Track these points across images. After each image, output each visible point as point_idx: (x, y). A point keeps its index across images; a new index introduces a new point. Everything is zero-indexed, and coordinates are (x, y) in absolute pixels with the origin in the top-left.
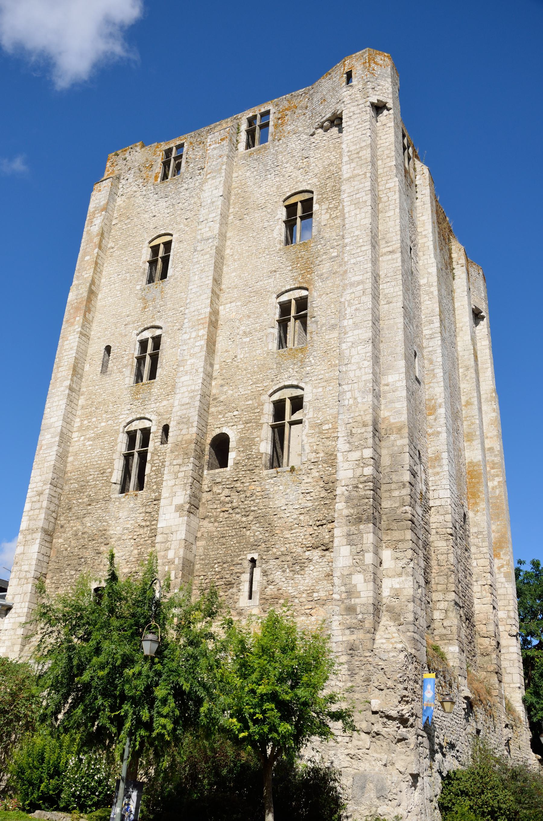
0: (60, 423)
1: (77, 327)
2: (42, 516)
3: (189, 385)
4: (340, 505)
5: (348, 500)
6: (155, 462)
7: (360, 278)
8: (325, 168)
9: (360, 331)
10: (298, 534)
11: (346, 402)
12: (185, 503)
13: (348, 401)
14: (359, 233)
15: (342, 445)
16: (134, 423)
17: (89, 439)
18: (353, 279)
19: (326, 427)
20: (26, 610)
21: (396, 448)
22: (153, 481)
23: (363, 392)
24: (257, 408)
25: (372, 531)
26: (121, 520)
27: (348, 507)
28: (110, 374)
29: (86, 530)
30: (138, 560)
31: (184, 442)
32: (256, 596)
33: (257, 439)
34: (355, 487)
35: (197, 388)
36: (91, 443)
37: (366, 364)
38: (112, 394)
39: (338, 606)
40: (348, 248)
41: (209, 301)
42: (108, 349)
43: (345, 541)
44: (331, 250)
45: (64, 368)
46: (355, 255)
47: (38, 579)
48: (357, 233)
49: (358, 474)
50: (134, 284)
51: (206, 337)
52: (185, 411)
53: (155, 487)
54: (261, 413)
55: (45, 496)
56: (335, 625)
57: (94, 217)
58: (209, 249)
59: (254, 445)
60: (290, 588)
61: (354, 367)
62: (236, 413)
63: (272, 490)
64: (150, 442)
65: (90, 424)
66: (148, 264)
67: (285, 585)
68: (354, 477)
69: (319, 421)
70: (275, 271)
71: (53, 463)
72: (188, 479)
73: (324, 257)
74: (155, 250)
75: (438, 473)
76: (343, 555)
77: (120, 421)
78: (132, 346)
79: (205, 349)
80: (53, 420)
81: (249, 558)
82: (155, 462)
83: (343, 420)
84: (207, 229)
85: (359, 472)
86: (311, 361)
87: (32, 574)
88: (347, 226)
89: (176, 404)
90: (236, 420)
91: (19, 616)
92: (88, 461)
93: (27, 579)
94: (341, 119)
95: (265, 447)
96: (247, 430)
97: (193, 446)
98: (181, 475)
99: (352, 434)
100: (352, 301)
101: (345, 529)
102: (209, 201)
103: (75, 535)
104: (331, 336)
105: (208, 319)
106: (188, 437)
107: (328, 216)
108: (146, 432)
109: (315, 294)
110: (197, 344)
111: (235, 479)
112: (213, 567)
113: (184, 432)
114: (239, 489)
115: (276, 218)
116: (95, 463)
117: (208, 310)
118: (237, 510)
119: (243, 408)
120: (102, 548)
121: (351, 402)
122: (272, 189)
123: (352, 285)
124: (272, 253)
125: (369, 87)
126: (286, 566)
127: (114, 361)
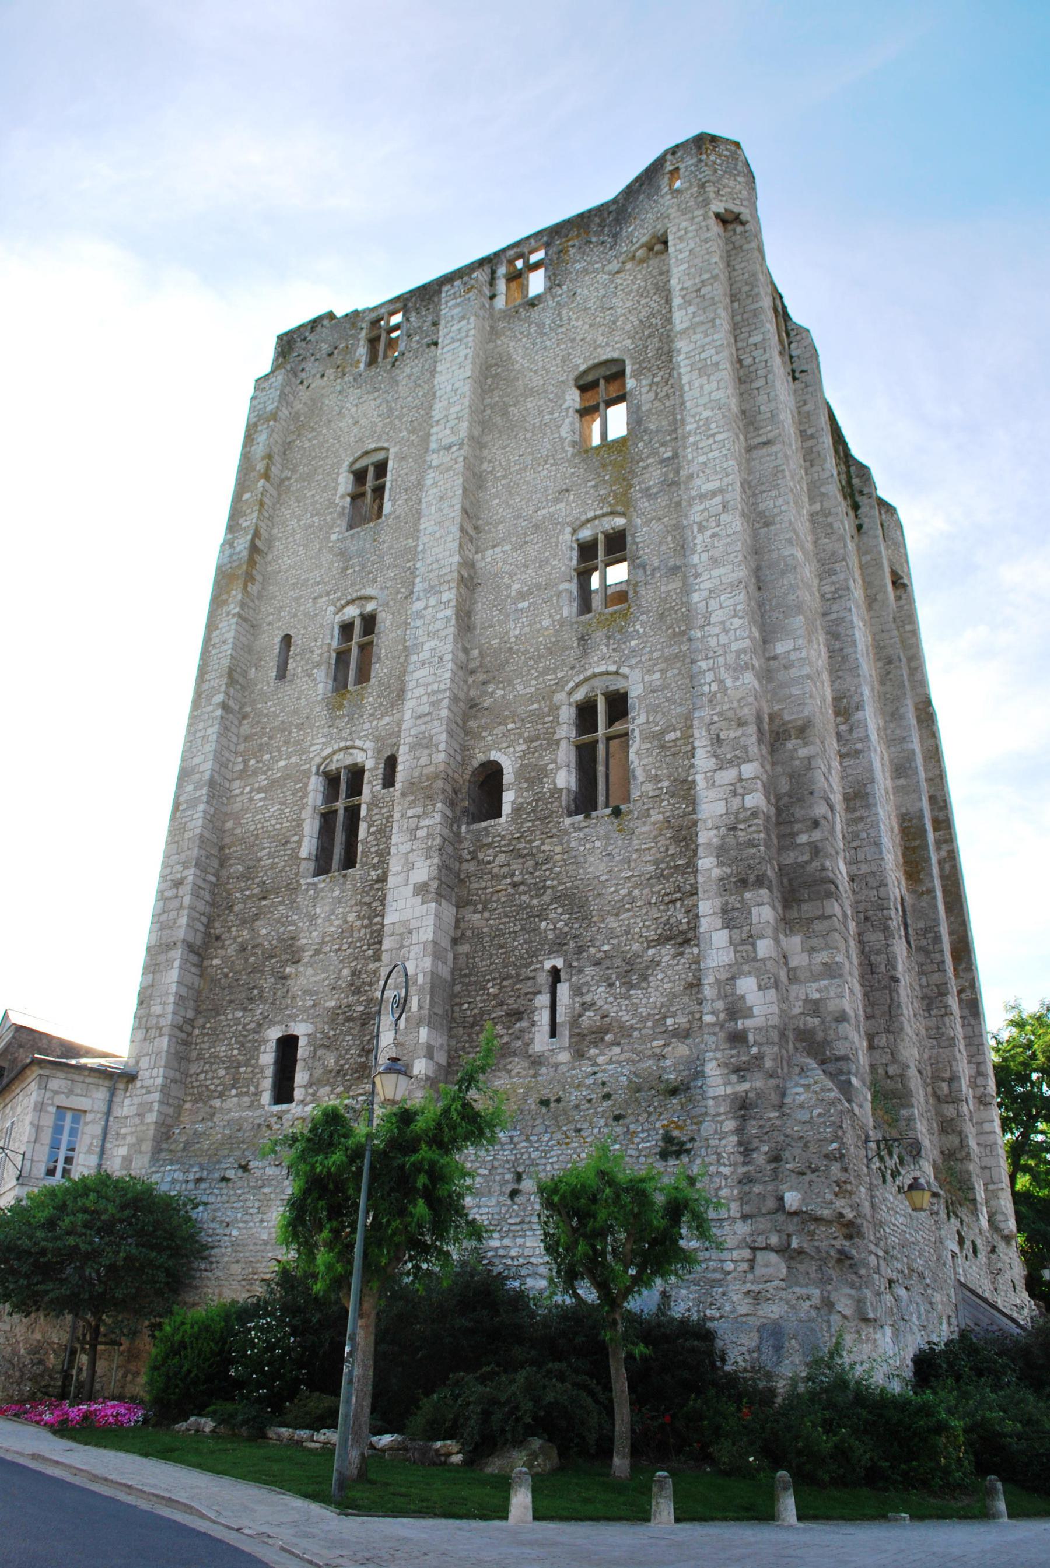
0: (209, 765)
2: (183, 921)
4: (706, 863)
5: (721, 851)
8: (641, 321)
9: (722, 571)
11: (706, 688)
13: (708, 685)
15: (703, 760)
16: (335, 758)
17: (259, 790)
19: (671, 736)
20: (159, 1081)
21: (797, 762)
22: (373, 850)
23: (735, 670)
26: (320, 921)
27: (721, 864)
28: (292, 681)
29: (260, 940)
30: (352, 985)
32: (564, 1032)
34: (730, 829)
35: (443, 687)
36: (263, 795)
37: (737, 622)
38: (296, 712)
39: (714, 1034)
40: (692, 439)
42: (287, 640)
43: (718, 922)
44: (662, 449)
45: (213, 675)
46: (706, 450)
47: (180, 1029)
48: (706, 413)
51: (453, 603)
52: (423, 727)
53: (376, 860)
54: (556, 720)
55: (186, 889)
56: (711, 1069)
59: (546, 776)
61: (716, 630)
62: (511, 726)
64: (365, 787)
66: (348, 499)
70: (567, 490)
71: (198, 831)
73: (650, 461)
74: (360, 476)
75: (861, 819)
76: (717, 948)
78: (328, 632)
79: (453, 622)
81: (548, 965)
84: (448, 432)
85: (736, 802)
86: (637, 631)
87: (168, 1020)
88: (688, 404)
91: (149, 1092)
93: (161, 1029)
94: (665, 243)
95: (565, 779)
97: (440, 783)
98: (421, 833)
101: (718, 902)
102: (449, 388)
104: (670, 587)
105: (456, 574)
107: (652, 395)
108: (357, 774)
109: (639, 521)
110: (440, 615)
112: (484, 988)
116: (270, 829)
117: (456, 558)
118: (522, 888)
120: (288, 970)
121: (715, 687)
123: (703, 497)
126: (614, 977)
127: (298, 658)
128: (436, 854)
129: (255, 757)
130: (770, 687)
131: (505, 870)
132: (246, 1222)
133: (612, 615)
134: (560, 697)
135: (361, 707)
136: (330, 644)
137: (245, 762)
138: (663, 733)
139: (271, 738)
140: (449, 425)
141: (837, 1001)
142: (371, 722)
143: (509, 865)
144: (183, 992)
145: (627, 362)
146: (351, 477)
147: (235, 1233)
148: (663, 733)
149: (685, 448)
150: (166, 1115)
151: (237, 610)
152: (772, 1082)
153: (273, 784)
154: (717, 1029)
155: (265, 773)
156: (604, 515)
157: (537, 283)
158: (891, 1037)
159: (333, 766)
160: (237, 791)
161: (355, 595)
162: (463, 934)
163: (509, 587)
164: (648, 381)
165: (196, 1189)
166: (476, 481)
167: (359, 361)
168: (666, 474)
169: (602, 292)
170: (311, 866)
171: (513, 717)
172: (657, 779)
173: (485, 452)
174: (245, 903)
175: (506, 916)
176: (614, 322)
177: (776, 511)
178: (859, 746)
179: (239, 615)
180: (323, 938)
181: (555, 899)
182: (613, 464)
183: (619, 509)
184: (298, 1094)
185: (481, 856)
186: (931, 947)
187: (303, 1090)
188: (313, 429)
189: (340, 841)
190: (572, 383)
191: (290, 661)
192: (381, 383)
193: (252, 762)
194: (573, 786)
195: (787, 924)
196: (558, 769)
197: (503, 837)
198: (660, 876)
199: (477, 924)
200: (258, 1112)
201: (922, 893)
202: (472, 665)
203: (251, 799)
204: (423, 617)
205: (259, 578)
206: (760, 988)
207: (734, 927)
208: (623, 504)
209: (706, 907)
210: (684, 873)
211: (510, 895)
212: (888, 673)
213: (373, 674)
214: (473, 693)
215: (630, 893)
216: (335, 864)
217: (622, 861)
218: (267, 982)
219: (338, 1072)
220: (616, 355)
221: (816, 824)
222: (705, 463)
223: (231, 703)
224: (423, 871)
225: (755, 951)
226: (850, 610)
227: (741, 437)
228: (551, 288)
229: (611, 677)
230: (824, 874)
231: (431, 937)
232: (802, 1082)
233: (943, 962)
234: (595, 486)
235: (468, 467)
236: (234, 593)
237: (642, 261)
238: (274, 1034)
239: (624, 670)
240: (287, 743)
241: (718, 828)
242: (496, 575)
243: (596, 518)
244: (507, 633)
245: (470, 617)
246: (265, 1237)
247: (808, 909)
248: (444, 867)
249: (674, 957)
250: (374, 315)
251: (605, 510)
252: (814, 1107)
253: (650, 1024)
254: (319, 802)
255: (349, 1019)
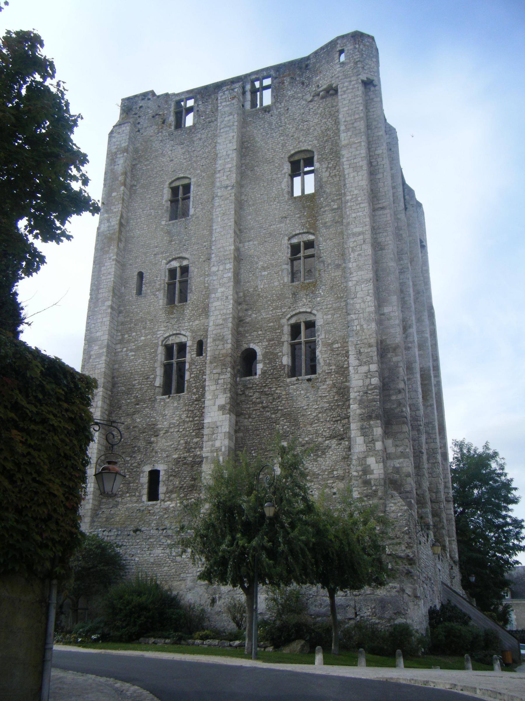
0: (106, 337)
1: (112, 255)
3: (221, 310)
4: (354, 407)
5: (361, 402)
6: (193, 370)
7: (361, 229)
9: (363, 273)
10: (318, 428)
12: (226, 404)
14: (358, 192)
15: (353, 360)
16: (171, 338)
17: (131, 350)
18: (355, 230)
19: (336, 346)
21: (392, 363)
22: (193, 385)
23: (368, 321)
24: (278, 329)
25: (380, 425)
26: (167, 417)
27: (361, 408)
28: (145, 296)
29: (136, 424)
30: (186, 448)
31: (221, 356)
33: (280, 354)
34: (365, 393)
35: (228, 312)
36: (133, 353)
37: (369, 298)
38: (148, 313)
39: (357, 480)
40: (349, 204)
41: (233, 240)
42: (141, 275)
43: (359, 433)
44: (332, 203)
45: (104, 290)
46: (356, 211)
48: (356, 192)
49: (367, 384)
50: (159, 220)
51: (232, 270)
52: (219, 331)
53: (195, 390)
54: (282, 332)
57: (116, 158)
58: (229, 196)
59: (277, 358)
60: (315, 468)
61: (360, 301)
62: (260, 332)
63: (295, 394)
65: (131, 338)
66: (169, 202)
67: (311, 466)
68: (363, 386)
69: (330, 341)
70: (286, 218)
71: (103, 370)
72: (227, 385)
73: (326, 208)
74: (175, 191)
76: (359, 444)
77: (158, 336)
78: (163, 273)
79: (232, 280)
80: (99, 334)
82: (193, 370)
83: (352, 342)
84: (225, 178)
85: (367, 381)
86: (320, 293)
88: (347, 185)
89: (211, 324)
90: (261, 338)
92: (132, 368)
95: (286, 360)
96: (271, 347)
97: (229, 359)
98: (220, 381)
99: (360, 353)
100: (355, 248)
101: (359, 424)
102: (225, 153)
103: (127, 429)
104: (336, 274)
105: (233, 256)
106: (224, 351)
107: (327, 174)
108: (182, 347)
109: (321, 239)
110: (225, 276)
111: (264, 385)
112: (250, 453)
113: (220, 347)
114: (268, 393)
115: (283, 172)
116: (138, 370)
117: (233, 247)
118: (267, 409)
119: (266, 328)
120: (152, 439)
121: (358, 327)
122: (278, 147)
124: (282, 202)
125: (359, 66)
127: (148, 285)
128: (228, 392)
129: (128, 334)
130: (381, 327)
131: (258, 400)
132: (142, 554)
133: (308, 284)
134: (284, 321)
135: (183, 314)
136: (164, 280)
137: (123, 335)
138: (332, 344)
139: (135, 325)
140: (226, 174)
141: (407, 468)
142: (189, 322)
143: (260, 398)
144: (100, 447)
145: (315, 153)
146: (170, 190)
147: (137, 559)
148: (332, 344)
149: (346, 208)
150: (95, 505)
151: (115, 257)
152: (381, 501)
153: (138, 349)
154: (358, 478)
155: (134, 342)
156: (304, 233)
157: (267, 98)
158: (419, 478)
159: (170, 342)
160: (119, 350)
161: (177, 256)
162: (239, 428)
163: (257, 263)
164: (326, 166)
165: (115, 539)
166: (240, 206)
167: (170, 125)
168: (334, 217)
169: (302, 111)
170: (161, 390)
171: (261, 329)
172: (329, 365)
173: (243, 190)
174: (127, 405)
175: (260, 422)
176: (309, 129)
177: (386, 243)
178: (410, 345)
179: (116, 260)
180: (170, 425)
181: (283, 415)
182: (309, 207)
183: (311, 231)
184: (161, 496)
185: (247, 393)
186: (431, 432)
187: (163, 495)
188: (148, 160)
189: (174, 379)
190: (287, 159)
191: (144, 286)
192: (184, 139)
193: (126, 336)
194: (290, 364)
195: (387, 434)
196: (283, 355)
197: (258, 385)
198: (331, 409)
199: (246, 424)
200: (141, 505)
201: (428, 406)
202: (240, 300)
203: (127, 355)
204: (217, 275)
205: (123, 239)
206: (377, 462)
207: (366, 436)
208: (313, 229)
209: (353, 426)
210: (341, 409)
211: (261, 412)
212: (417, 298)
213: (189, 299)
214: (240, 314)
215: (317, 416)
216: (173, 391)
217: (313, 401)
218: (141, 444)
219: (181, 487)
220: (309, 148)
221: (400, 392)
222: (355, 217)
223: (114, 305)
224: (223, 399)
225: (375, 447)
226: (408, 279)
227: (371, 204)
228: (275, 103)
229: (308, 314)
230: (403, 414)
231: (228, 430)
232: (393, 501)
233: (436, 438)
234: (299, 217)
235: (237, 198)
236: (112, 247)
237: (323, 98)
238: (147, 469)
239: (314, 312)
240: (145, 328)
241: (359, 392)
242: (251, 256)
243: (300, 234)
244: (257, 286)
245: (238, 276)
246: (152, 561)
247: (395, 428)
248: (232, 398)
249: (337, 445)
250: (178, 98)
251: (305, 231)
252: (398, 512)
253: (326, 473)
254: (163, 359)
255: (185, 464)
